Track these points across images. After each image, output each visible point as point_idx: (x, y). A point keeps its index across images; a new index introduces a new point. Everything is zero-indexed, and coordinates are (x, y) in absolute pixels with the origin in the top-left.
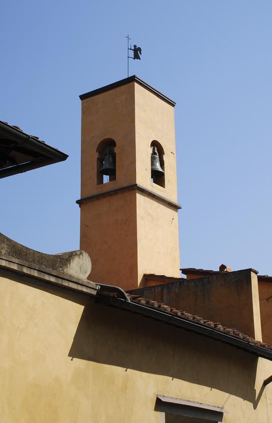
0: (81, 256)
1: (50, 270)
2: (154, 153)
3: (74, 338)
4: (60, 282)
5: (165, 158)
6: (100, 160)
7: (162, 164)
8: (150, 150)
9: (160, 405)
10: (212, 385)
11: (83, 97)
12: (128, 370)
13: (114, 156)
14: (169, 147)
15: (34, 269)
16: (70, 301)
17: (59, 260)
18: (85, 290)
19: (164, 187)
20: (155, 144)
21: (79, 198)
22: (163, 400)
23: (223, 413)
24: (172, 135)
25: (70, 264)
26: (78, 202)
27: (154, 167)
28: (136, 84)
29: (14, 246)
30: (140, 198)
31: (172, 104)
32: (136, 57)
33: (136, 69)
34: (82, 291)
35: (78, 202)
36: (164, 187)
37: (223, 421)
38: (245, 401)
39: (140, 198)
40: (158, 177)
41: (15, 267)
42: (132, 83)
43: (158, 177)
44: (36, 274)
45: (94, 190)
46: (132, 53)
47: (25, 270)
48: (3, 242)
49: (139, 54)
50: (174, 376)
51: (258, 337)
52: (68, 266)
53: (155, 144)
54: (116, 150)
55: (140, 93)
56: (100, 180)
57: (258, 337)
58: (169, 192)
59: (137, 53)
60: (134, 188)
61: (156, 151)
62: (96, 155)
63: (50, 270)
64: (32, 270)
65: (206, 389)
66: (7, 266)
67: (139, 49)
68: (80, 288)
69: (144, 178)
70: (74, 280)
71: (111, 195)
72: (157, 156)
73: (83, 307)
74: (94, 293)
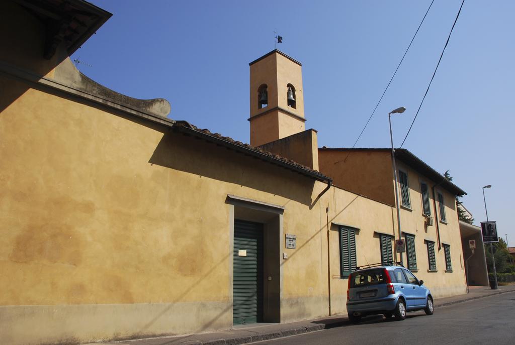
0: (162, 102)
1: (135, 108)
2: (289, 90)
3: (154, 152)
4: (140, 115)
5: (296, 93)
6: (260, 96)
7: (294, 96)
8: (287, 89)
9: (229, 200)
10: (275, 193)
11: (250, 64)
12: (202, 177)
13: (266, 93)
14: (299, 88)
15: (117, 104)
16: (151, 129)
17: (143, 102)
18: (162, 122)
19: (296, 108)
20: (289, 85)
21: (249, 118)
22: (231, 197)
23: (283, 210)
24: (300, 81)
25: (152, 106)
26: (248, 120)
27: (289, 98)
28: (277, 53)
29: (103, 90)
30: (280, 114)
31: (301, 65)
32: (280, 41)
33: (279, 47)
34: (159, 123)
35: (248, 120)
36: (296, 108)
37: (156, 167)
38: (303, 204)
39: (280, 114)
40: (292, 103)
41: (101, 101)
42: (274, 54)
43: (292, 103)
44: (119, 107)
45: (257, 113)
46: (277, 40)
47: (109, 104)
48: (95, 86)
49: (468, 225)
50: (242, 185)
51: (316, 167)
52: (151, 107)
53: (289, 85)
54: (267, 90)
55: (278, 57)
56: (260, 107)
57: (316, 167)
58: (299, 111)
59: (280, 39)
60: (277, 109)
61: (291, 89)
62: (258, 94)
63: (135, 108)
64: (116, 105)
65: (271, 195)
66: (94, 99)
67: (281, 38)
68: (158, 121)
69: (282, 103)
70: (153, 115)
71: (265, 114)
72: (291, 92)
73: (162, 134)
74: (171, 125)
